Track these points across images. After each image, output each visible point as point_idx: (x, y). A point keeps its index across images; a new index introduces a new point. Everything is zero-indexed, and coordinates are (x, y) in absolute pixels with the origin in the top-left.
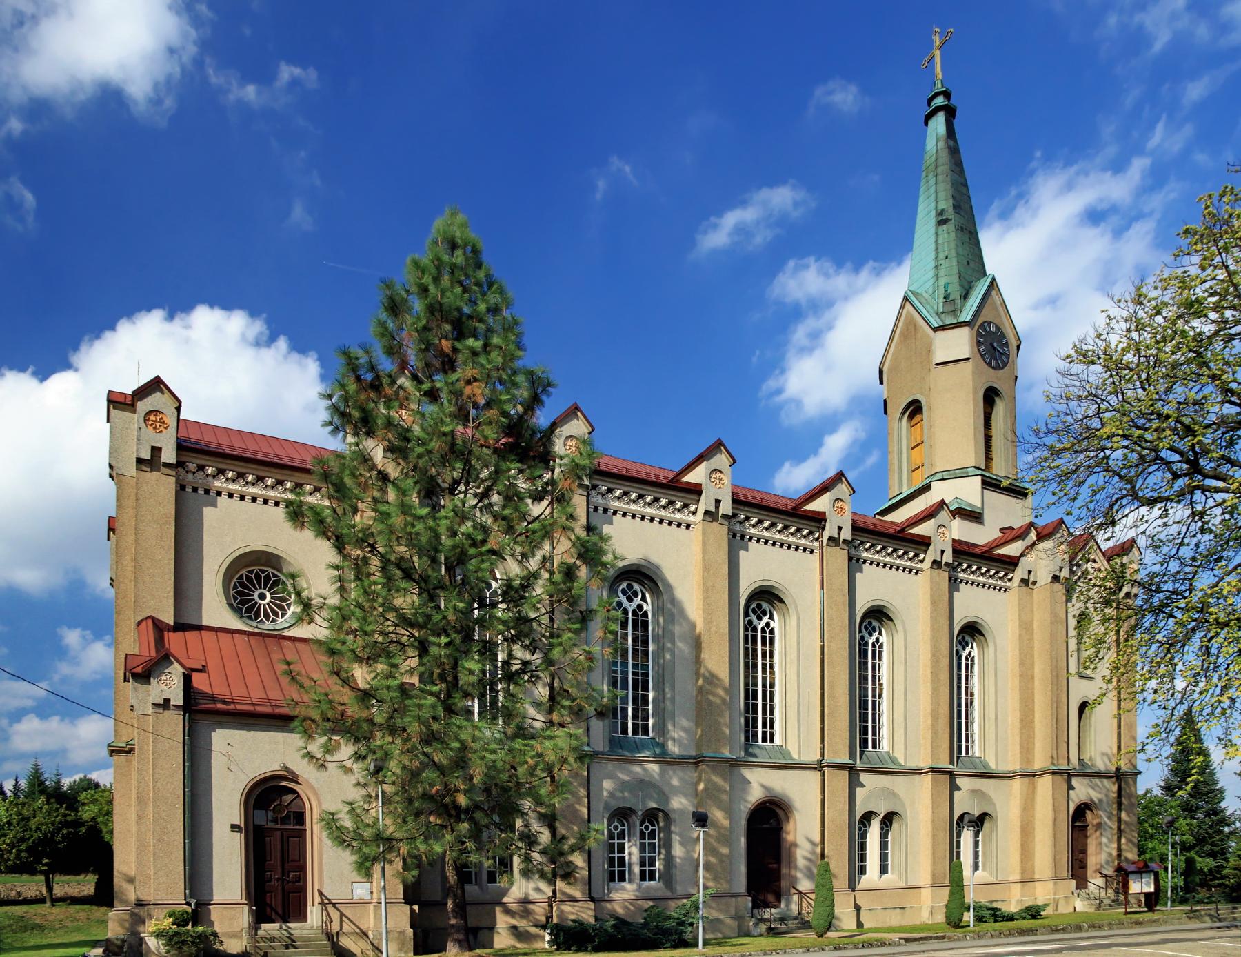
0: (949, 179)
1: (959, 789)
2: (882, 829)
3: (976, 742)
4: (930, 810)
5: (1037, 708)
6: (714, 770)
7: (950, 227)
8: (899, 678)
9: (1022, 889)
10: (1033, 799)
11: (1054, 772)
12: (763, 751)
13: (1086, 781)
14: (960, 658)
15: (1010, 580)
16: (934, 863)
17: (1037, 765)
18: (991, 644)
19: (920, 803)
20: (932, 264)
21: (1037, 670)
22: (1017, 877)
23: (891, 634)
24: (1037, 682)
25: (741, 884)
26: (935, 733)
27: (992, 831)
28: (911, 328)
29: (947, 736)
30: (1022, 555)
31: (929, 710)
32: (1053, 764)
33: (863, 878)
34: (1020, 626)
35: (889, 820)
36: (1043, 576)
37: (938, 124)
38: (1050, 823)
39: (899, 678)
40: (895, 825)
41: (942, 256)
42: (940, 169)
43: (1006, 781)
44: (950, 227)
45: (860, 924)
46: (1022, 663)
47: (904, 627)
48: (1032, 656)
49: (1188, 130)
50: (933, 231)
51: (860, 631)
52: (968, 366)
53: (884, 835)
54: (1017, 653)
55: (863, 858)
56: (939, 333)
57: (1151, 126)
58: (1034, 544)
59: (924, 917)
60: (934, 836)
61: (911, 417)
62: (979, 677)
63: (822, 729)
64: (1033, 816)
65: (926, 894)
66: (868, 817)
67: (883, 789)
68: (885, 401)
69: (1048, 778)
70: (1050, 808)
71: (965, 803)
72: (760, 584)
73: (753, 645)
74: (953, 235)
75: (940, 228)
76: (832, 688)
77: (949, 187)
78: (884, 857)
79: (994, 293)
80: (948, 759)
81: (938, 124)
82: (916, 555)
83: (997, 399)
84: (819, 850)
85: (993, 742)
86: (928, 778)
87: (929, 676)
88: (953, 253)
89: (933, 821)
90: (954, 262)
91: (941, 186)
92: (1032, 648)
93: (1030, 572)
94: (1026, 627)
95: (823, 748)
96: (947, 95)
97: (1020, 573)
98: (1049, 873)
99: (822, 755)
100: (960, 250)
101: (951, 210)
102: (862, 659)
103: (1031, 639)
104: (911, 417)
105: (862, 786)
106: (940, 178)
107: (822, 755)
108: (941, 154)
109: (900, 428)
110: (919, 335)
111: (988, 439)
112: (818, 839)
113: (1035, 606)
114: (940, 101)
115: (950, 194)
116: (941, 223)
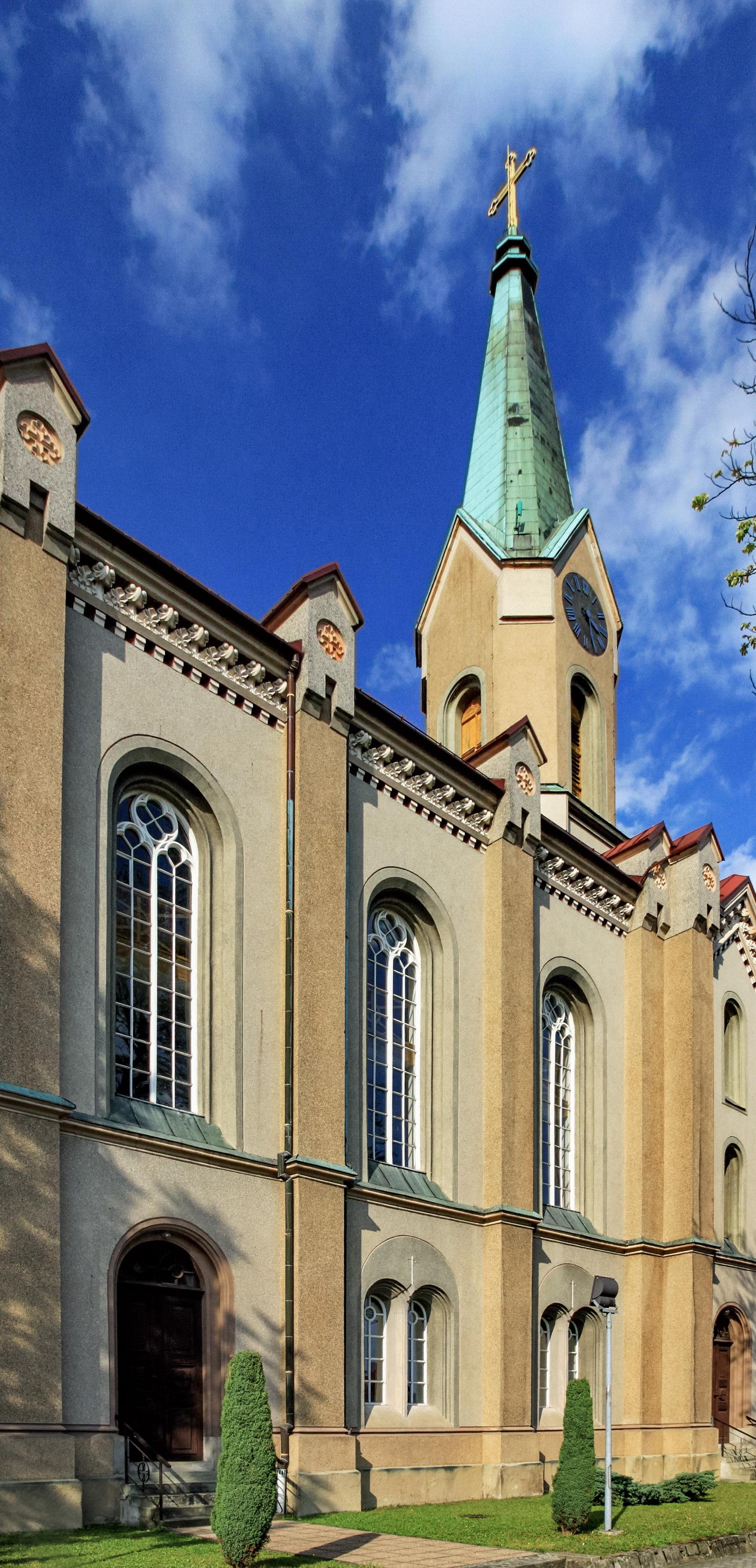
1: (547, 1260)
2: (411, 1318)
3: (572, 1187)
4: (499, 1289)
5: (667, 1139)
6: (19, 1124)
7: (527, 430)
8: (445, 1036)
9: (644, 1441)
10: (660, 1292)
11: (697, 1248)
12: (157, 1122)
13: (734, 1271)
14: (547, 1031)
15: (628, 916)
16: (506, 1388)
17: (667, 1237)
18: (597, 1018)
19: (479, 1271)
20: (499, 481)
21: (669, 1076)
22: (634, 1419)
23: (432, 946)
24: (668, 1098)
25: (99, 1404)
26: (508, 1149)
27: (596, 1340)
28: (466, 565)
30: (648, 874)
31: (498, 1103)
32: (697, 1236)
33: (376, 1409)
34: (644, 996)
35: (424, 1300)
36: (680, 918)
38: (689, 1333)
39: (445, 1036)
40: (436, 1313)
41: (513, 469)
42: (512, 348)
43: (618, 1258)
44: (527, 430)
45: (368, 1502)
46: (646, 1060)
47: (454, 939)
48: (661, 1053)
49: (711, 756)
50: (500, 433)
51: (372, 930)
53: (415, 1331)
54: (639, 1040)
55: (375, 1371)
56: (508, 571)
57: (680, 749)
58: (664, 863)
59: (488, 1485)
60: (506, 1338)
61: (464, 706)
62: (578, 1075)
63: (289, 1092)
64: (660, 1320)
65: (492, 1443)
66: (383, 1291)
67: (414, 1239)
68: (424, 682)
69: (687, 1259)
70: (689, 1307)
71: (554, 1287)
72: (152, 744)
73: (139, 898)
74: (530, 443)
75: (512, 430)
76: (311, 1009)
77: (525, 374)
78: (415, 1372)
80: (530, 1200)
82: (477, 809)
83: (588, 699)
84: (282, 1340)
85: (599, 1188)
86: (496, 1230)
87: (498, 1038)
89: (504, 1311)
90: (531, 480)
91: (514, 372)
92: (662, 1037)
93: (660, 907)
94: (652, 999)
95: (290, 1132)
96: (522, 245)
97: (643, 906)
98: (684, 1415)
99: (289, 1146)
102: (372, 996)
103: (660, 1023)
104: (464, 706)
105: (374, 1228)
106: (513, 360)
107: (289, 1146)
108: (514, 327)
112: (279, 1318)
113: (666, 968)
114: (514, 253)
115: (527, 384)
116: (515, 422)
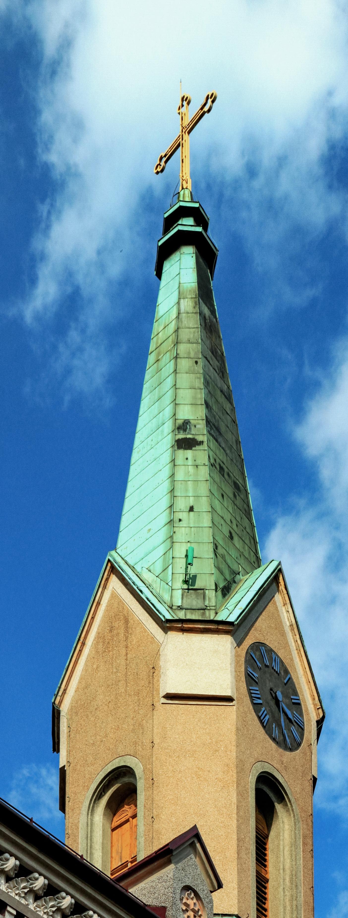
0: (199, 368)
7: (201, 455)
20: (164, 518)
28: (119, 624)
29: (255, 592)
37: (183, 266)
41: (182, 504)
42: (183, 348)
44: (201, 455)
50: (167, 457)
52: (229, 714)
74: (204, 472)
75: (181, 454)
77: (199, 383)
79: (278, 598)
81: (183, 266)
88: (203, 505)
90: (206, 521)
96: (197, 215)
100: (217, 505)
101: (202, 426)
104: (114, 807)
106: (184, 364)
109: (90, 825)
110: (134, 640)
111: (262, 883)
115: (201, 396)
116: (185, 444)
